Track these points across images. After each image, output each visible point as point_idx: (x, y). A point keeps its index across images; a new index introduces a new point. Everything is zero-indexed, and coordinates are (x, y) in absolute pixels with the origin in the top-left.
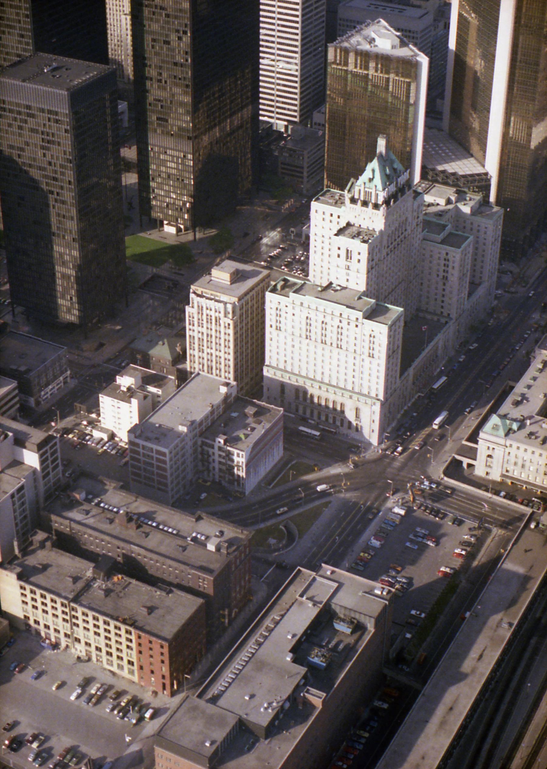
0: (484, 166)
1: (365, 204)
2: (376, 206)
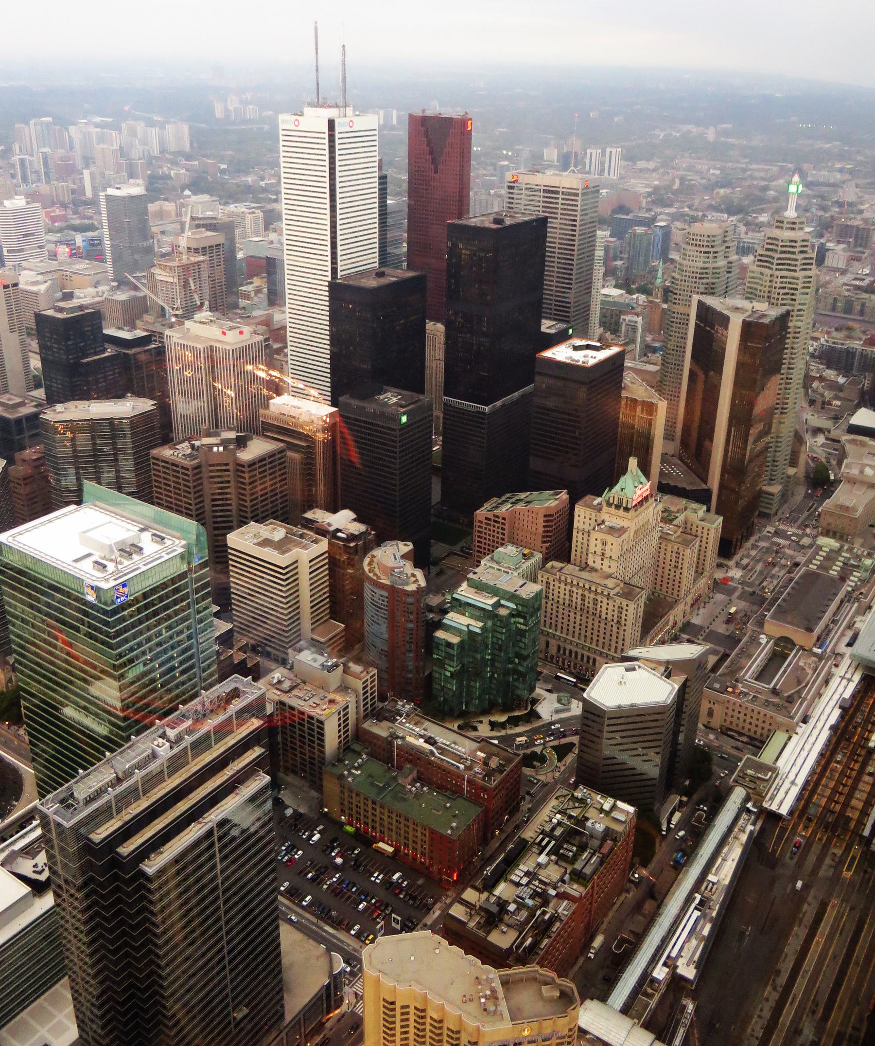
0: (705, 482)
1: (618, 507)
2: (627, 509)
